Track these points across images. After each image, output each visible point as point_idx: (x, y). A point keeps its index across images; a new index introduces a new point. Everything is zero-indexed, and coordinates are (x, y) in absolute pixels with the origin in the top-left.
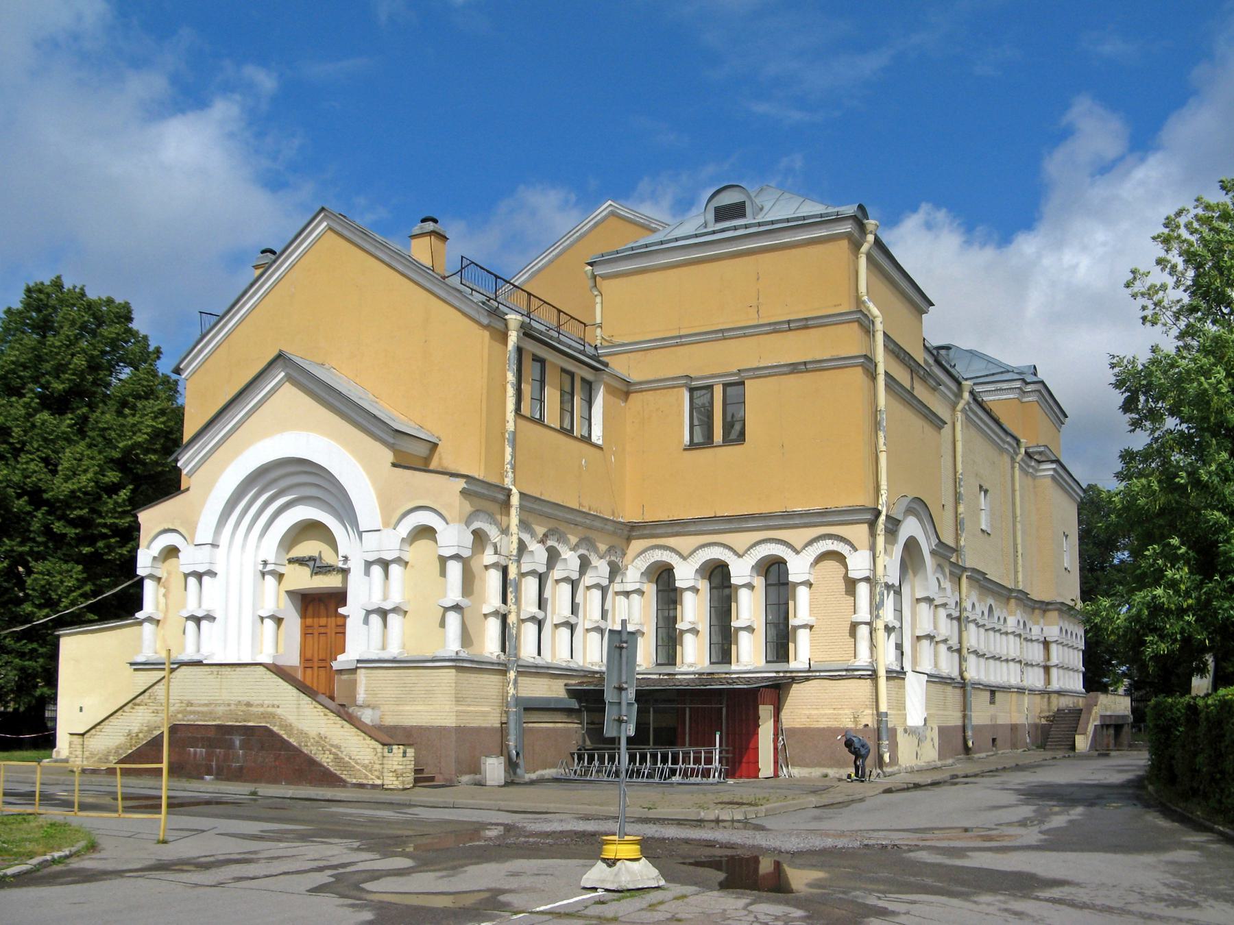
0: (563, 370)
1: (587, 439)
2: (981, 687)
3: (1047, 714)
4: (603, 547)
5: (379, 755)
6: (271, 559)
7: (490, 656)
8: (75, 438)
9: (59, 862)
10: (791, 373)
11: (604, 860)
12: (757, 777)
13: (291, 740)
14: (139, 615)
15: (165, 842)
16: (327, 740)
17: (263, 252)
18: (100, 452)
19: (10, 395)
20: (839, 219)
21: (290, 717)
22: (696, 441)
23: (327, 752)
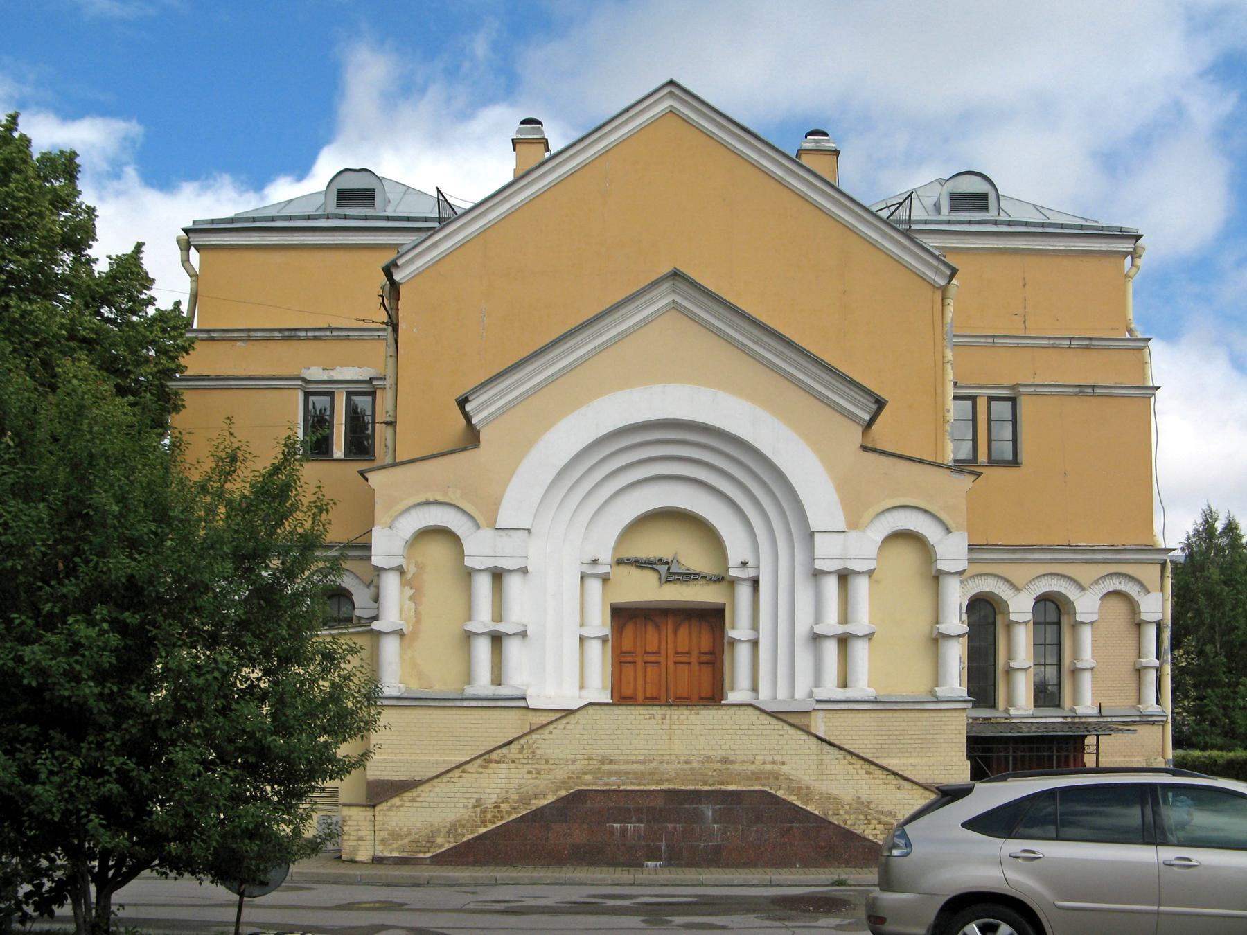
10: (1076, 395)
13: (809, 808)
16: (872, 806)
21: (805, 778)
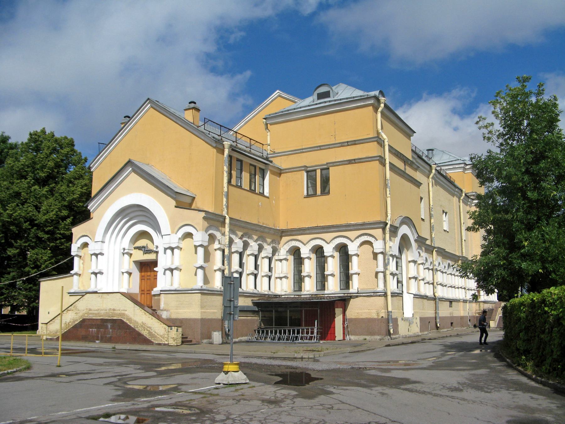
0: (251, 165)
1: (262, 194)
2: (444, 300)
3: (479, 312)
4: (269, 240)
5: (167, 331)
6: (127, 247)
7: (217, 288)
8: (50, 197)
9: (11, 374)
11: (224, 372)
12: (335, 340)
13: (131, 325)
14: (72, 272)
15: (59, 366)
17: (125, 117)
18: (59, 203)
19: (21, 179)
20: (369, 98)
22: (310, 193)
23: (146, 330)
